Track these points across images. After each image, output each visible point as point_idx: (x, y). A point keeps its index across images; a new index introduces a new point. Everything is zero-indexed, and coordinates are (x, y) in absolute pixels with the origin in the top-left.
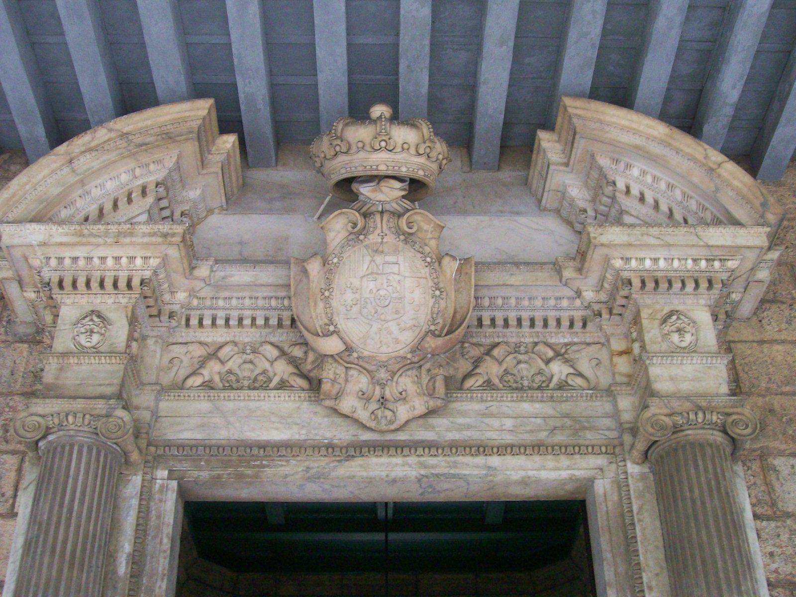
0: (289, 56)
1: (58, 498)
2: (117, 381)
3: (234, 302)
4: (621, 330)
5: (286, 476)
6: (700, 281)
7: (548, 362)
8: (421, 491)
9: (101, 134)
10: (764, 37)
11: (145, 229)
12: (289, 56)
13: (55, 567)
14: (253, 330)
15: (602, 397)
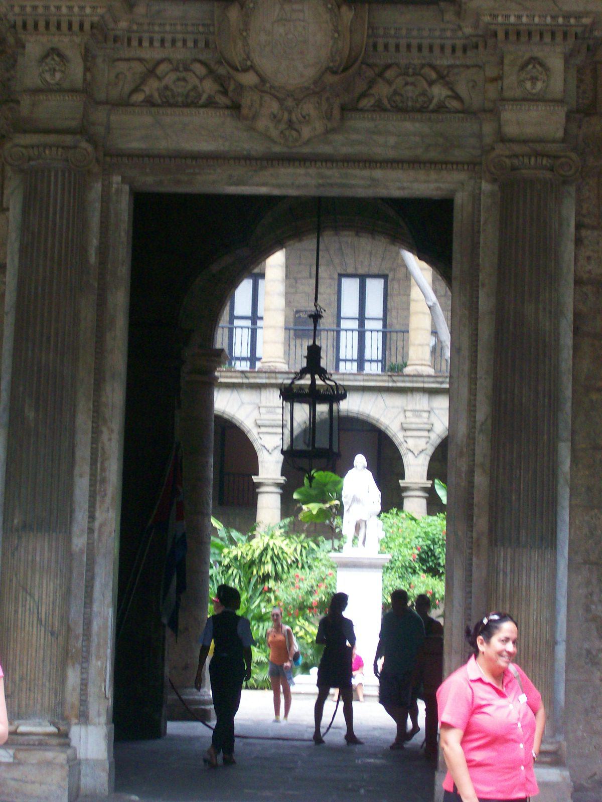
3: (168, 28)
7: (431, 83)
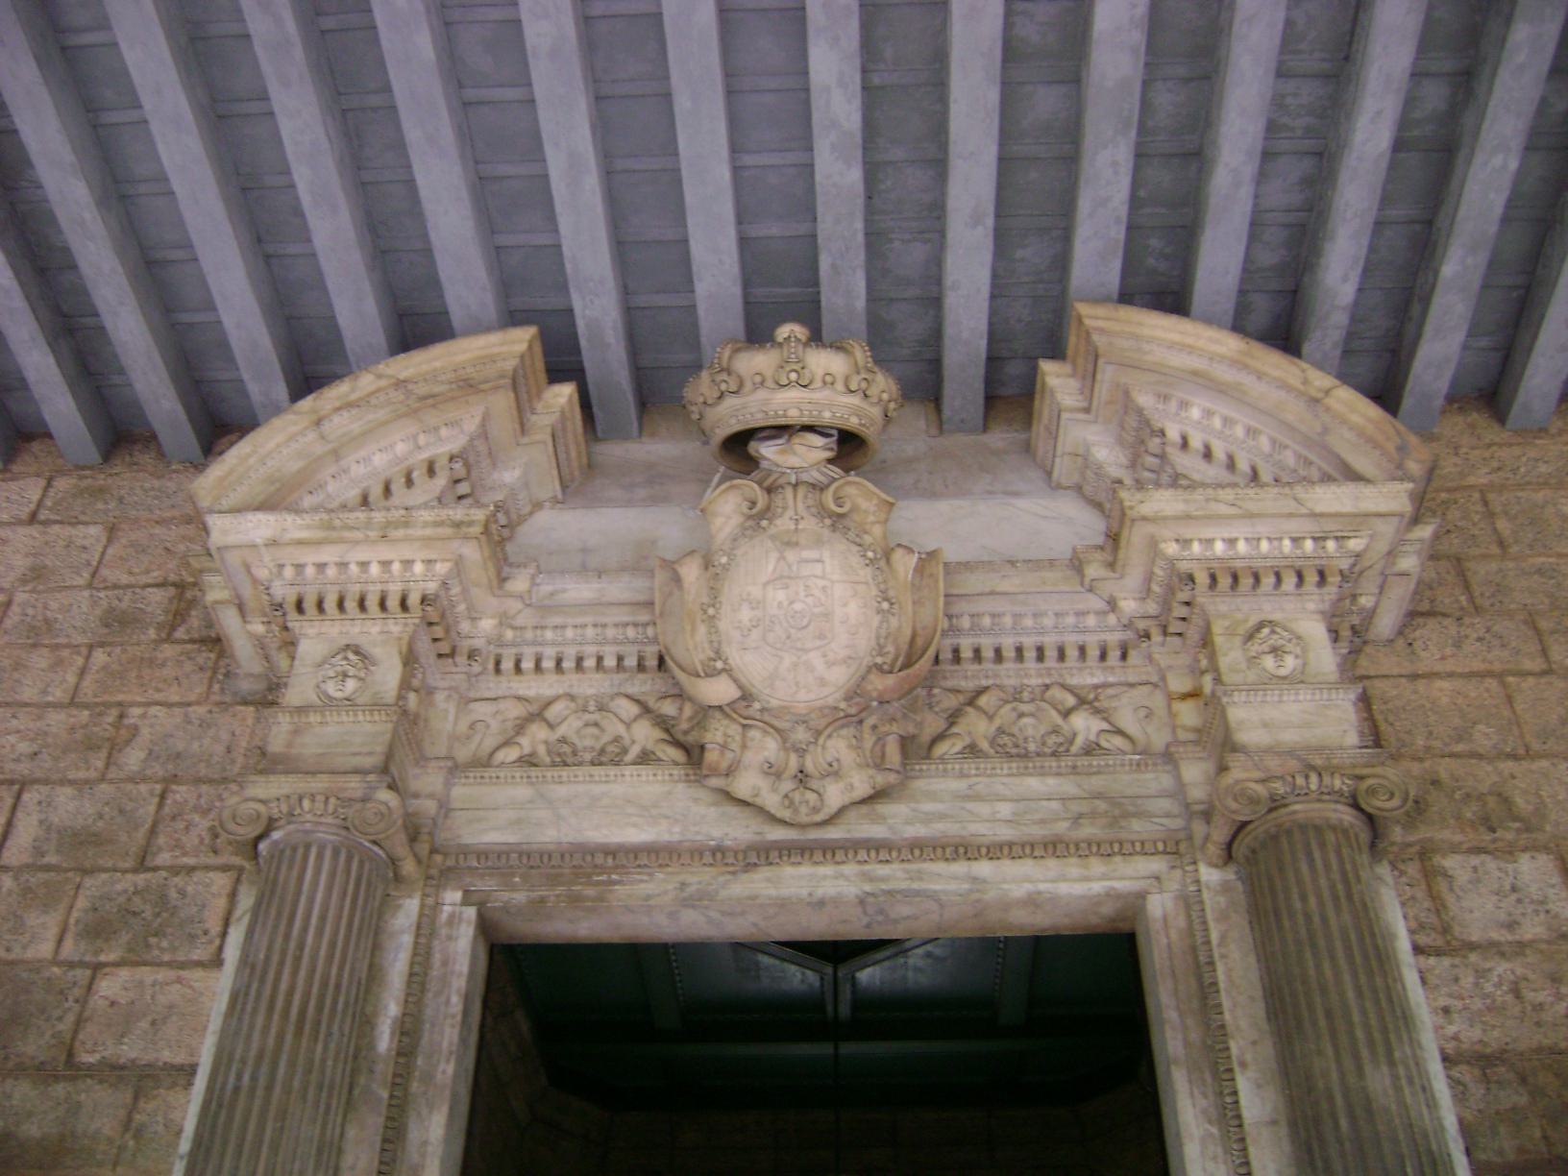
0: (650, 258)
1: (282, 928)
2: (380, 749)
3: (570, 633)
4: (1184, 660)
5: (648, 897)
6: (1305, 573)
7: (1066, 714)
8: (865, 920)
9: (366, 382)
10: (1386, 200)
11: (426, 515)
12: (650, 258)
13: (273, 1031)
14: (598, 676)
15: (1155, 765)
